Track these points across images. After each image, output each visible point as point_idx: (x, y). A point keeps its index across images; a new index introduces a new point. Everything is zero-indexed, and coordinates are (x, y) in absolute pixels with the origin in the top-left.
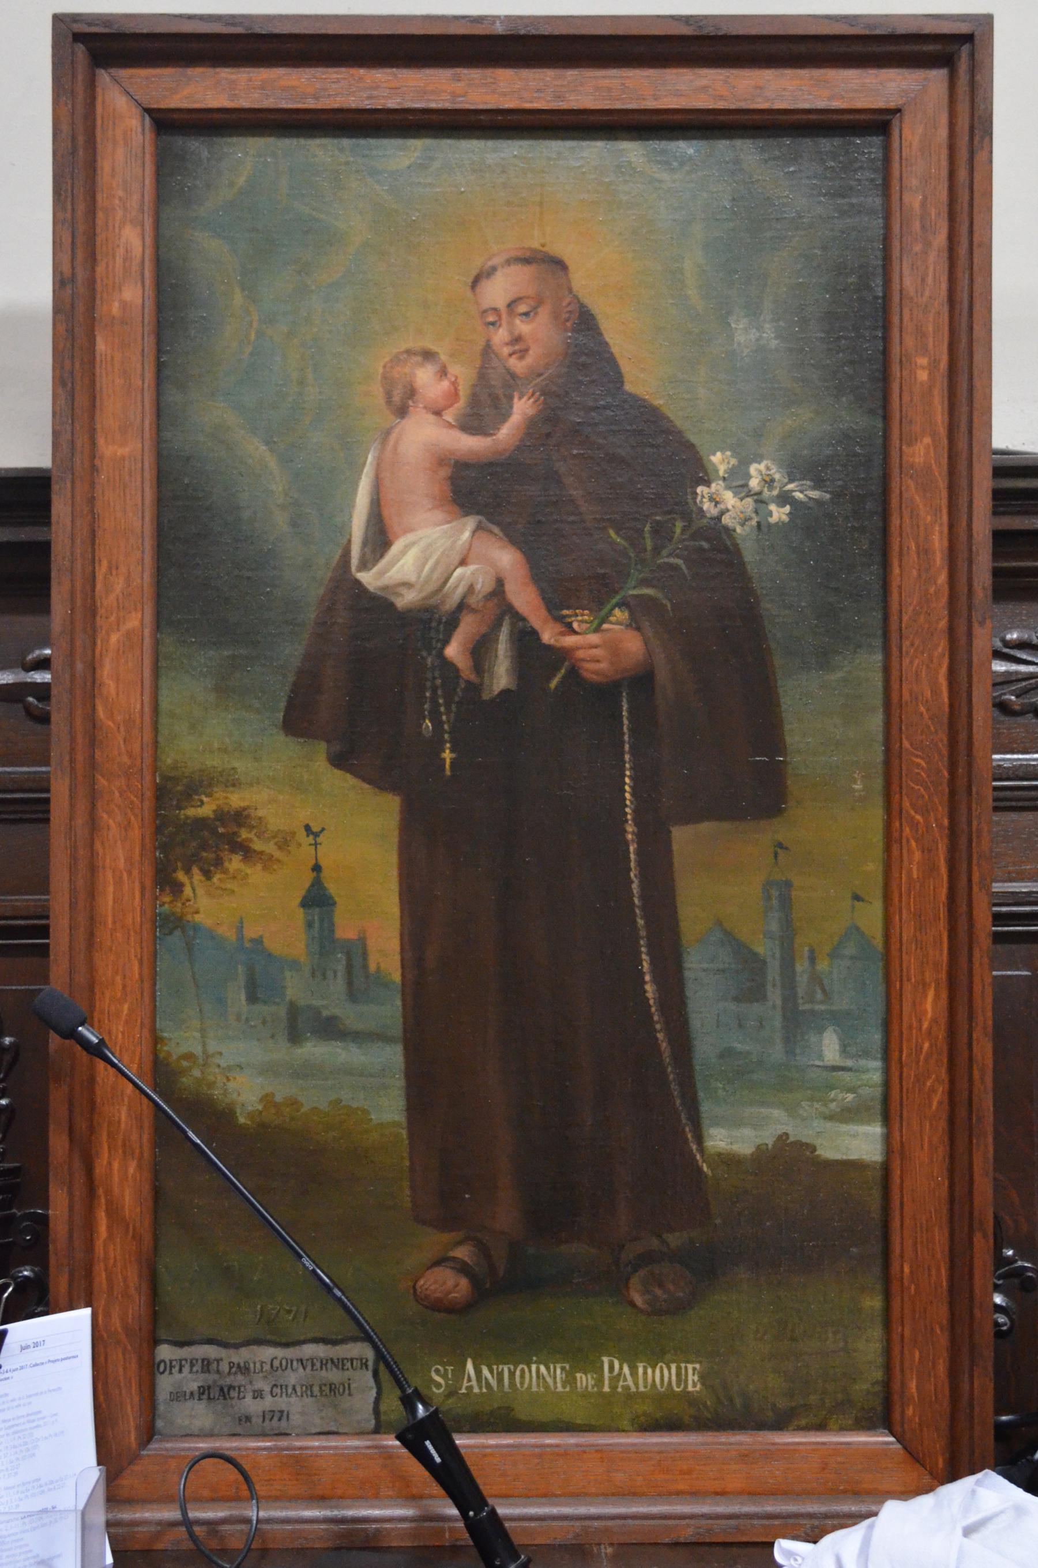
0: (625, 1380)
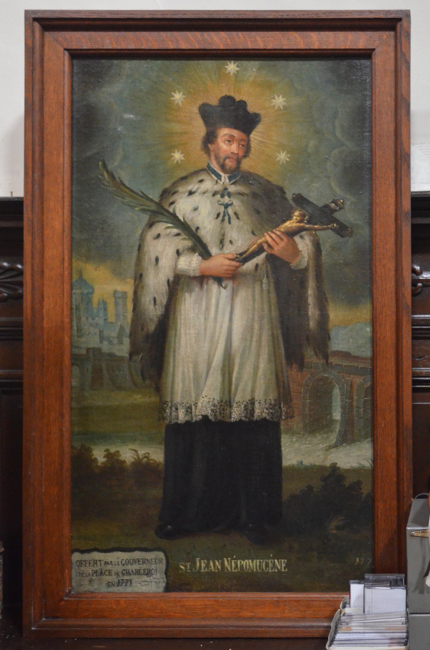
0: (211, 568)
